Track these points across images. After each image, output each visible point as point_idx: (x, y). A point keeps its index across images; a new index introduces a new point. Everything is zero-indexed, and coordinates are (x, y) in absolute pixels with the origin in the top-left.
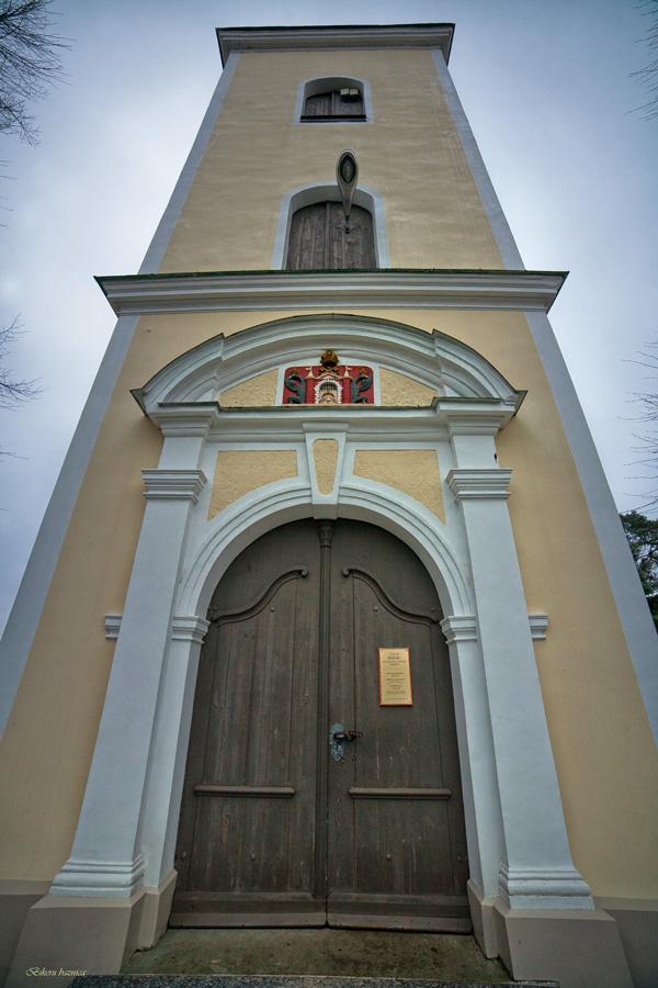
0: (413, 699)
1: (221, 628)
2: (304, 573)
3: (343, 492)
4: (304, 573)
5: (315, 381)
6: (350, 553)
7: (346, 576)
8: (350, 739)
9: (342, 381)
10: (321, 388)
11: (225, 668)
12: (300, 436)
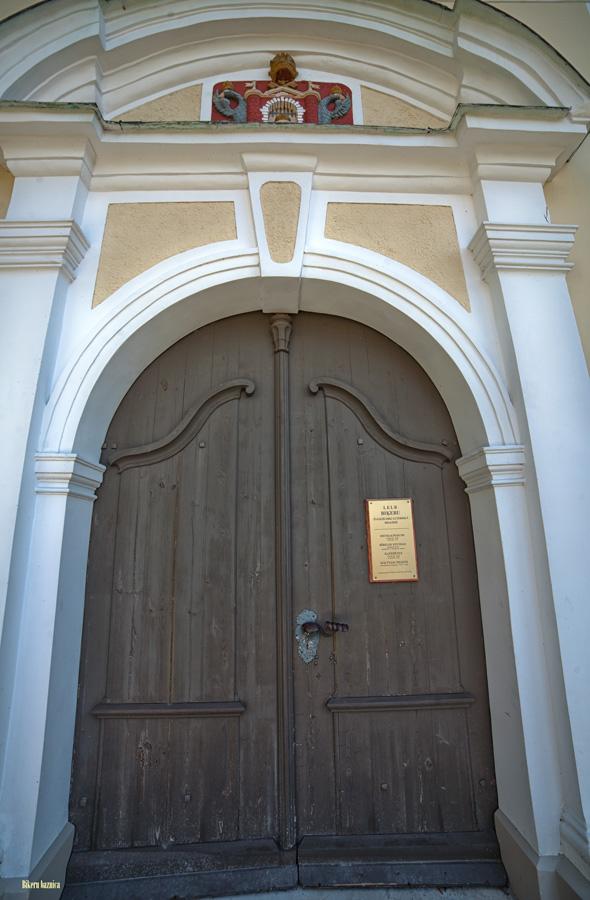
0: (419, 573)
1: (123, 475)
2: (249, 390)
3: (310, 260)
4: (249, 390)
5: (263, 101)
6: (311, 362)
7: (315, 394)
8: (325, 629)
9: (304, 102)
10: (271, 113)
11: (132, 535)
12: (240, 179)
